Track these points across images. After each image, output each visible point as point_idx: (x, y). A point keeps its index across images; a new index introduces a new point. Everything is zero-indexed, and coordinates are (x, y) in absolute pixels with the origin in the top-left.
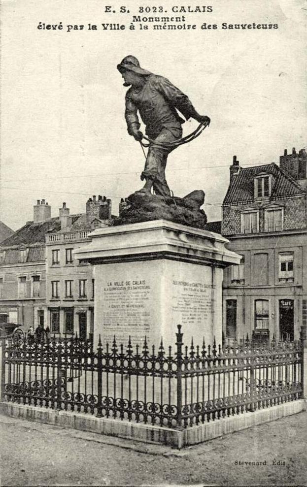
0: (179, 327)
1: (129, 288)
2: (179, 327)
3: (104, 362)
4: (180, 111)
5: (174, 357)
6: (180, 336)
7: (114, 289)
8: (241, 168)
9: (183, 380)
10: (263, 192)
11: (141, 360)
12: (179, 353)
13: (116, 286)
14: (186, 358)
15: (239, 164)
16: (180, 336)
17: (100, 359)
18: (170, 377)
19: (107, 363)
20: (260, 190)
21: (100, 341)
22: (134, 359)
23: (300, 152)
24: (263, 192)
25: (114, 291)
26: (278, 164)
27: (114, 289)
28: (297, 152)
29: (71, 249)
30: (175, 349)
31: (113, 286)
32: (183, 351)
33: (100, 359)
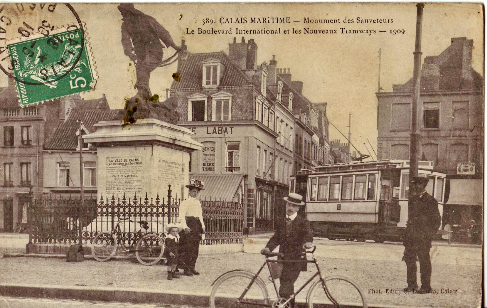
0: (170, 186)
1: (126, 164)
2: (170, 186)
3: (116, 210)
4: (439, 214)
5: (166, 203)
6: (170, 191)
7: (114, 164)
8: (190, 54)
9: (171, 218)
10: (211, 80)
11: (121, 207)
12: (169, 202)
13: (116, 162)
14: (173, 205)
15: (188, 49)
16: (170, 191)
17: (113, 208)
18: (107, 216)
19: (119, 210)
20: (208, 78)
21: (102, 197)
22: (105, 207)
23: (249, 41)
24: (211, 80)
25: (114, 166)
26: (227, 53)
27: (114, 164)
28: (247, 42)
29: (28, 127)
30: (167, 199)
31: (114, 162)
32: (172, 201)
33: (113, 208)
